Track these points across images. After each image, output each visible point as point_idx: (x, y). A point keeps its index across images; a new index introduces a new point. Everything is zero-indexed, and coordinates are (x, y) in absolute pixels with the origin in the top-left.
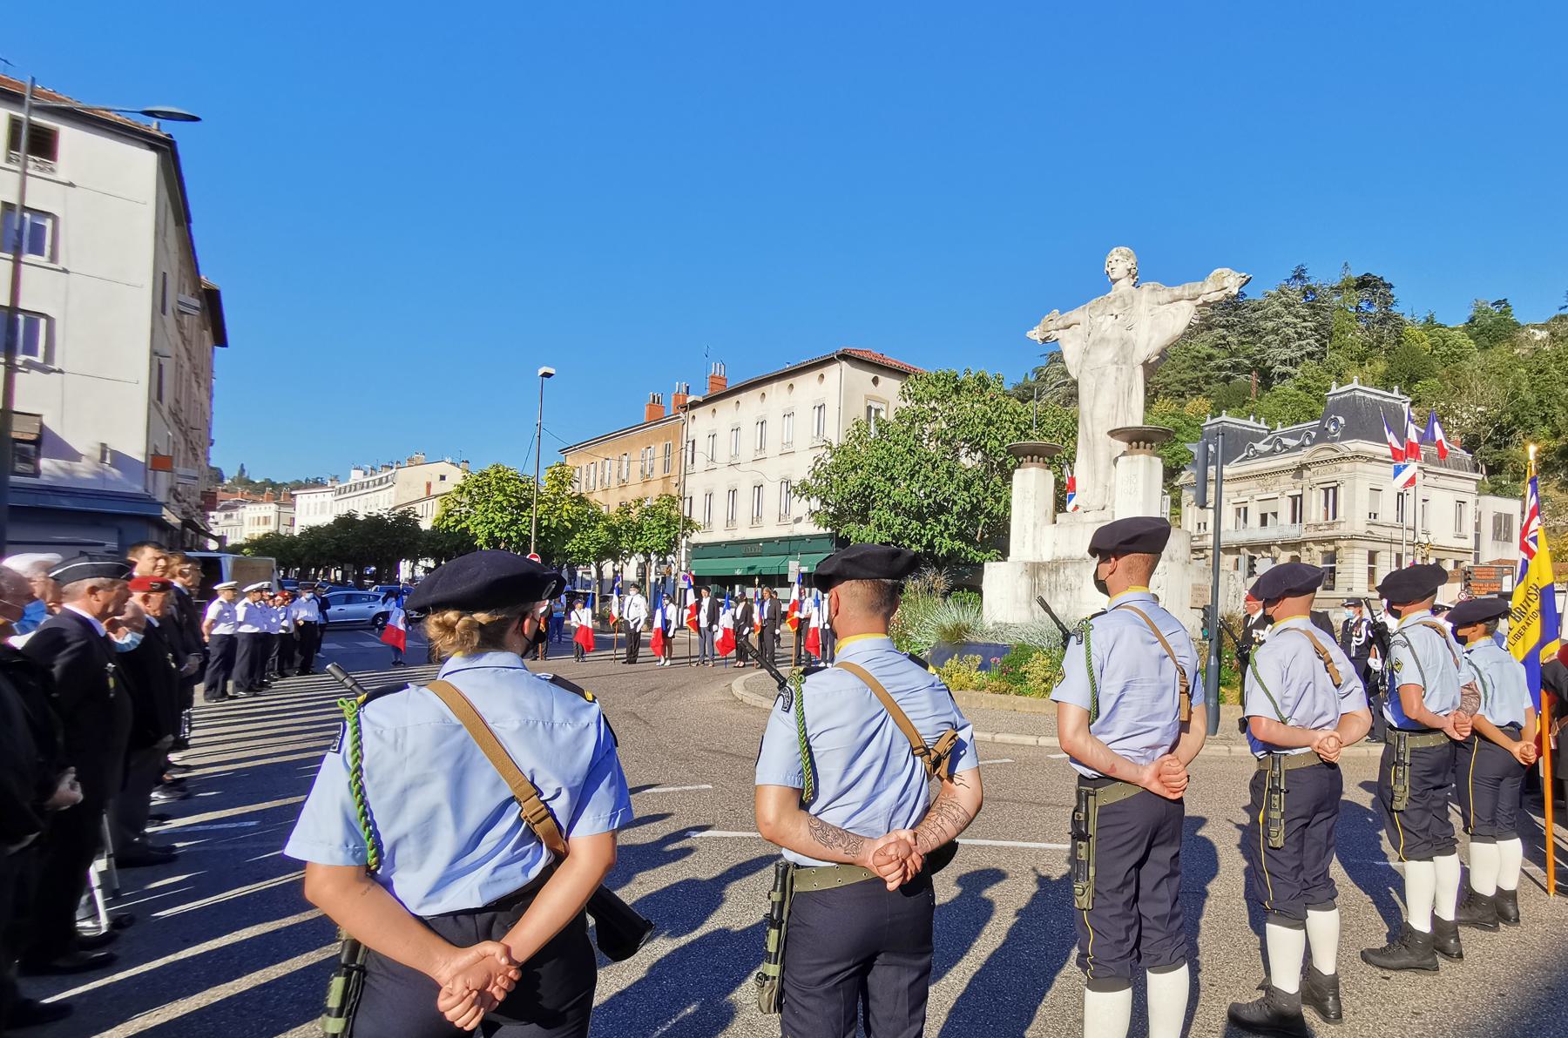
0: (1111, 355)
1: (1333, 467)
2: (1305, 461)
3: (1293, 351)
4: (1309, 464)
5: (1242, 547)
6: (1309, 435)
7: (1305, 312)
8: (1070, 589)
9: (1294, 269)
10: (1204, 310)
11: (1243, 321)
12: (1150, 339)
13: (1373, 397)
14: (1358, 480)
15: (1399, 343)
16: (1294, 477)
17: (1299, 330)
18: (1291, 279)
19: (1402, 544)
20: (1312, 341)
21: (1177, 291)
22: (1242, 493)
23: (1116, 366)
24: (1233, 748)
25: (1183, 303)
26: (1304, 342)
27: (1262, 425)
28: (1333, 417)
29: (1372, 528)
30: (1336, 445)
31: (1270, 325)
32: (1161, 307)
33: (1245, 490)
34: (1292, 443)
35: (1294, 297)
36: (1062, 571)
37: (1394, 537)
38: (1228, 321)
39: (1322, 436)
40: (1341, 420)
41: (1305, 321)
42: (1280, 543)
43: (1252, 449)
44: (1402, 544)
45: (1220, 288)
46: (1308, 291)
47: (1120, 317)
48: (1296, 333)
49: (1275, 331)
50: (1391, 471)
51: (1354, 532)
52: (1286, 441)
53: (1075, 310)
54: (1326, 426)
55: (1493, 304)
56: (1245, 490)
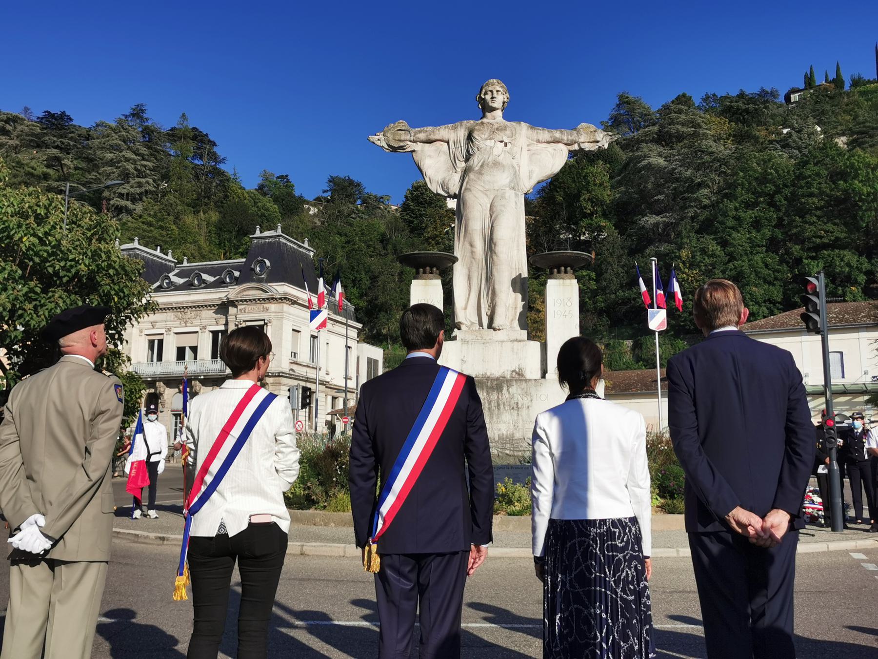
0: (508, 180)
1: (261, 307)
2: (232, 297)
3: (132, 187)
4: (237, 301)
5: (159, 381)
6: (230, 274)
7: (144, 150)
8: (517, 407)
9: (134, 107)
10: (33, 126)
11: (79, 146)
12: (531, 172)
13: (292, 245)
14: (284, 321)
15: (226, 197)
16: (216, 312)
17: (139, 167)
18: (129, 116)
19: (316, 383)
20: (151, 181)
21: (557, 134)
22: (158, 325)
23: (513, 191)
24: (675, 555)
25: (561, 145)
26: (143, 180)
27: (170, 257)
28: (260, 258)
29: (294, 367)
30: (266, 286)
31: (109, 156)
32: (539, 145)
33: (161, 321)
34: (209, 279)
35: (134, 133)
36: (505, 388)
37: (310, 375)
38: (63, 143)
39: (247, 276)
40: (268, 263)
41: (143, 159)
42: (202, 377)
43: (167, 281)
44: (316, 383)
45: (592, 140)
46: (148, 132)
47: (509, 145)
48: (136, 169)
49: (111, 163)
50: (308, 315)
51: (281, 370)
52: (205, 276)
53: (443, 127)
54: (253, 266)
55: (278, 178)
56: (161, 321)
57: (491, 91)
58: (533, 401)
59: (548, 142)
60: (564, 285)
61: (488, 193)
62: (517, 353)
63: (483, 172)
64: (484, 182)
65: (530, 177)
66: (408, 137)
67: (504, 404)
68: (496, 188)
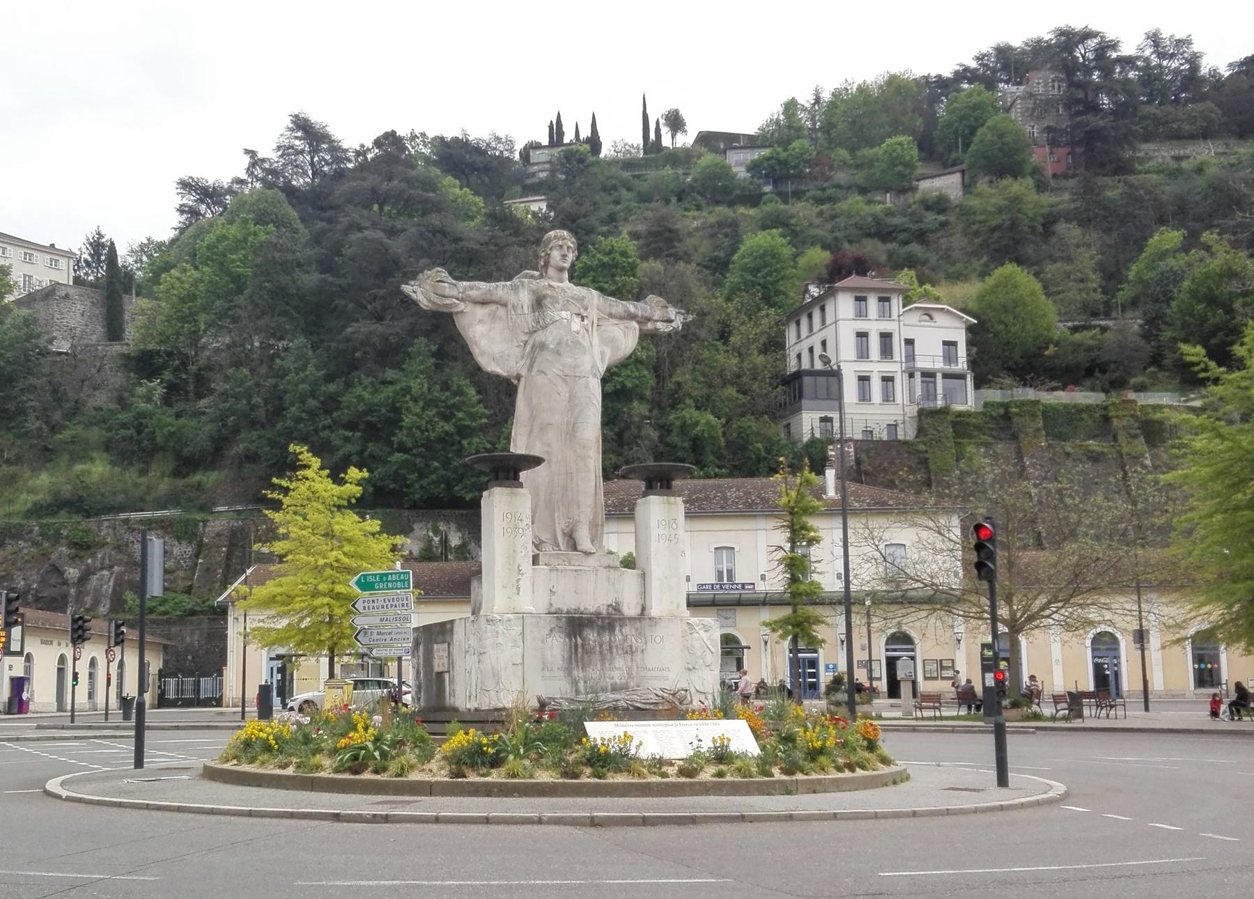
8: (630, 651)
58: (649, 643)
59: (621, 318)
60: (669, 503)
62: (613, 584)
65: (603, 360)
66: (455, 293)
67: (617, 647)
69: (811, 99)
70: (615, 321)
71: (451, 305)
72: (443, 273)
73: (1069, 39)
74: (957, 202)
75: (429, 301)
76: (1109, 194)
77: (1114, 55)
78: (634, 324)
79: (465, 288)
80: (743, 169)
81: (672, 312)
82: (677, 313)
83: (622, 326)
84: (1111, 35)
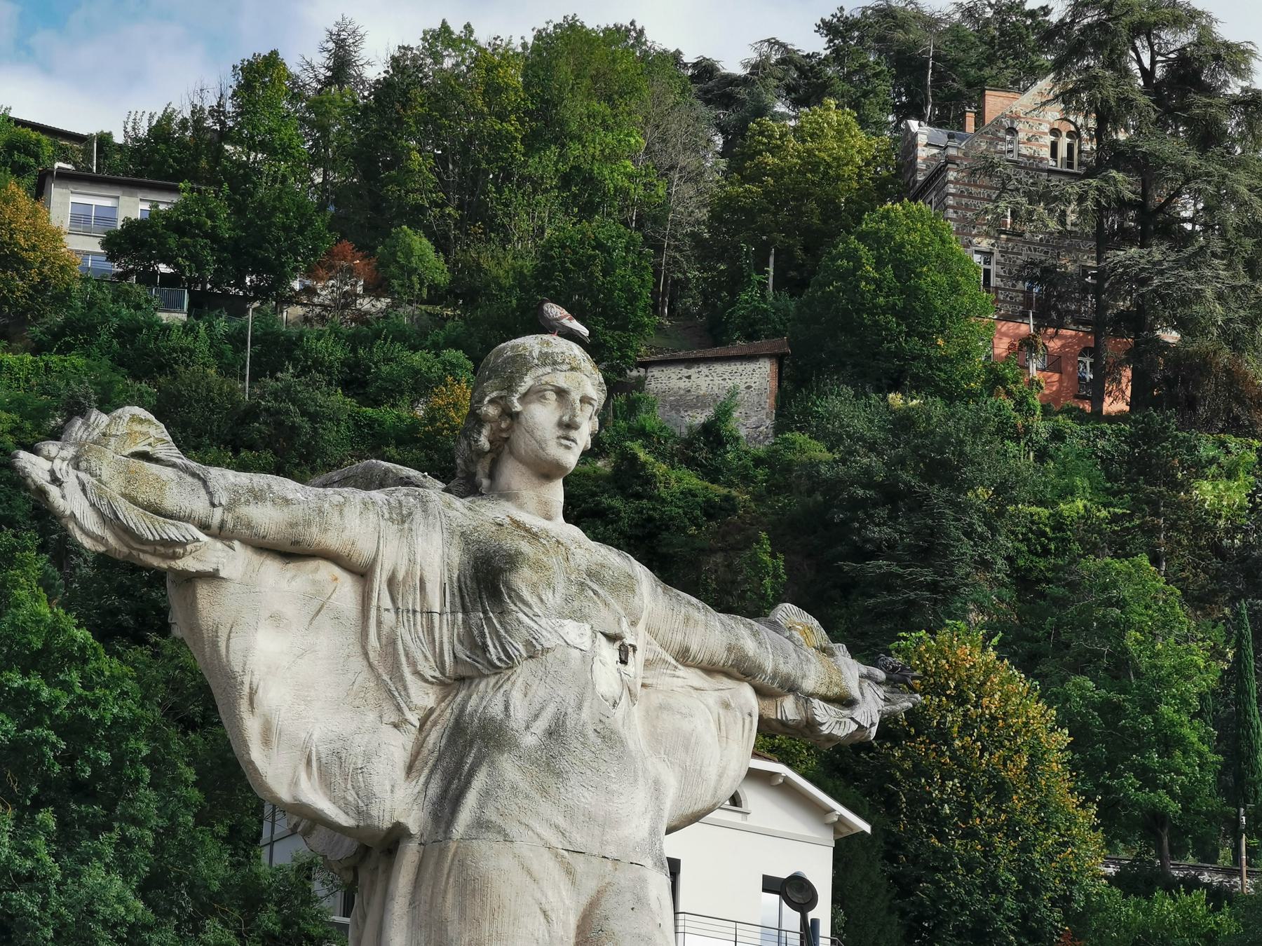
32: (682, 671)
57: (561, 393)
59: (710, 669)
61: (579, 863)
63: (563, 764)
64: (569, 813)
66: (198, 505)
68: (611, 851)
69: (321, 61)
70: (693, 677)
71: (170, 547)
72: (155, 435)
73: (886, 14)
74: (760, 449)
75: (111, 520)
76: (1206, 492)
77: (1235, 87)
78: (746, 693)
79: (235, 491)
80: (93, 245)
81: (850, 672)
82: (863, 677)
83: (712, 698)
84: (1227, 31)
